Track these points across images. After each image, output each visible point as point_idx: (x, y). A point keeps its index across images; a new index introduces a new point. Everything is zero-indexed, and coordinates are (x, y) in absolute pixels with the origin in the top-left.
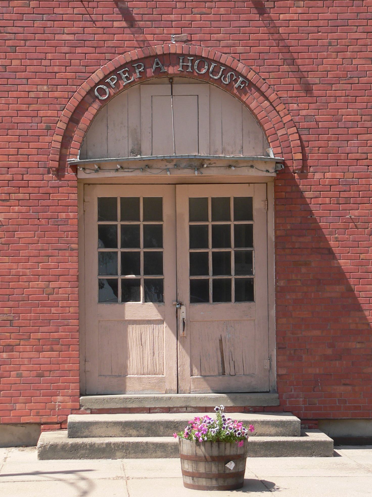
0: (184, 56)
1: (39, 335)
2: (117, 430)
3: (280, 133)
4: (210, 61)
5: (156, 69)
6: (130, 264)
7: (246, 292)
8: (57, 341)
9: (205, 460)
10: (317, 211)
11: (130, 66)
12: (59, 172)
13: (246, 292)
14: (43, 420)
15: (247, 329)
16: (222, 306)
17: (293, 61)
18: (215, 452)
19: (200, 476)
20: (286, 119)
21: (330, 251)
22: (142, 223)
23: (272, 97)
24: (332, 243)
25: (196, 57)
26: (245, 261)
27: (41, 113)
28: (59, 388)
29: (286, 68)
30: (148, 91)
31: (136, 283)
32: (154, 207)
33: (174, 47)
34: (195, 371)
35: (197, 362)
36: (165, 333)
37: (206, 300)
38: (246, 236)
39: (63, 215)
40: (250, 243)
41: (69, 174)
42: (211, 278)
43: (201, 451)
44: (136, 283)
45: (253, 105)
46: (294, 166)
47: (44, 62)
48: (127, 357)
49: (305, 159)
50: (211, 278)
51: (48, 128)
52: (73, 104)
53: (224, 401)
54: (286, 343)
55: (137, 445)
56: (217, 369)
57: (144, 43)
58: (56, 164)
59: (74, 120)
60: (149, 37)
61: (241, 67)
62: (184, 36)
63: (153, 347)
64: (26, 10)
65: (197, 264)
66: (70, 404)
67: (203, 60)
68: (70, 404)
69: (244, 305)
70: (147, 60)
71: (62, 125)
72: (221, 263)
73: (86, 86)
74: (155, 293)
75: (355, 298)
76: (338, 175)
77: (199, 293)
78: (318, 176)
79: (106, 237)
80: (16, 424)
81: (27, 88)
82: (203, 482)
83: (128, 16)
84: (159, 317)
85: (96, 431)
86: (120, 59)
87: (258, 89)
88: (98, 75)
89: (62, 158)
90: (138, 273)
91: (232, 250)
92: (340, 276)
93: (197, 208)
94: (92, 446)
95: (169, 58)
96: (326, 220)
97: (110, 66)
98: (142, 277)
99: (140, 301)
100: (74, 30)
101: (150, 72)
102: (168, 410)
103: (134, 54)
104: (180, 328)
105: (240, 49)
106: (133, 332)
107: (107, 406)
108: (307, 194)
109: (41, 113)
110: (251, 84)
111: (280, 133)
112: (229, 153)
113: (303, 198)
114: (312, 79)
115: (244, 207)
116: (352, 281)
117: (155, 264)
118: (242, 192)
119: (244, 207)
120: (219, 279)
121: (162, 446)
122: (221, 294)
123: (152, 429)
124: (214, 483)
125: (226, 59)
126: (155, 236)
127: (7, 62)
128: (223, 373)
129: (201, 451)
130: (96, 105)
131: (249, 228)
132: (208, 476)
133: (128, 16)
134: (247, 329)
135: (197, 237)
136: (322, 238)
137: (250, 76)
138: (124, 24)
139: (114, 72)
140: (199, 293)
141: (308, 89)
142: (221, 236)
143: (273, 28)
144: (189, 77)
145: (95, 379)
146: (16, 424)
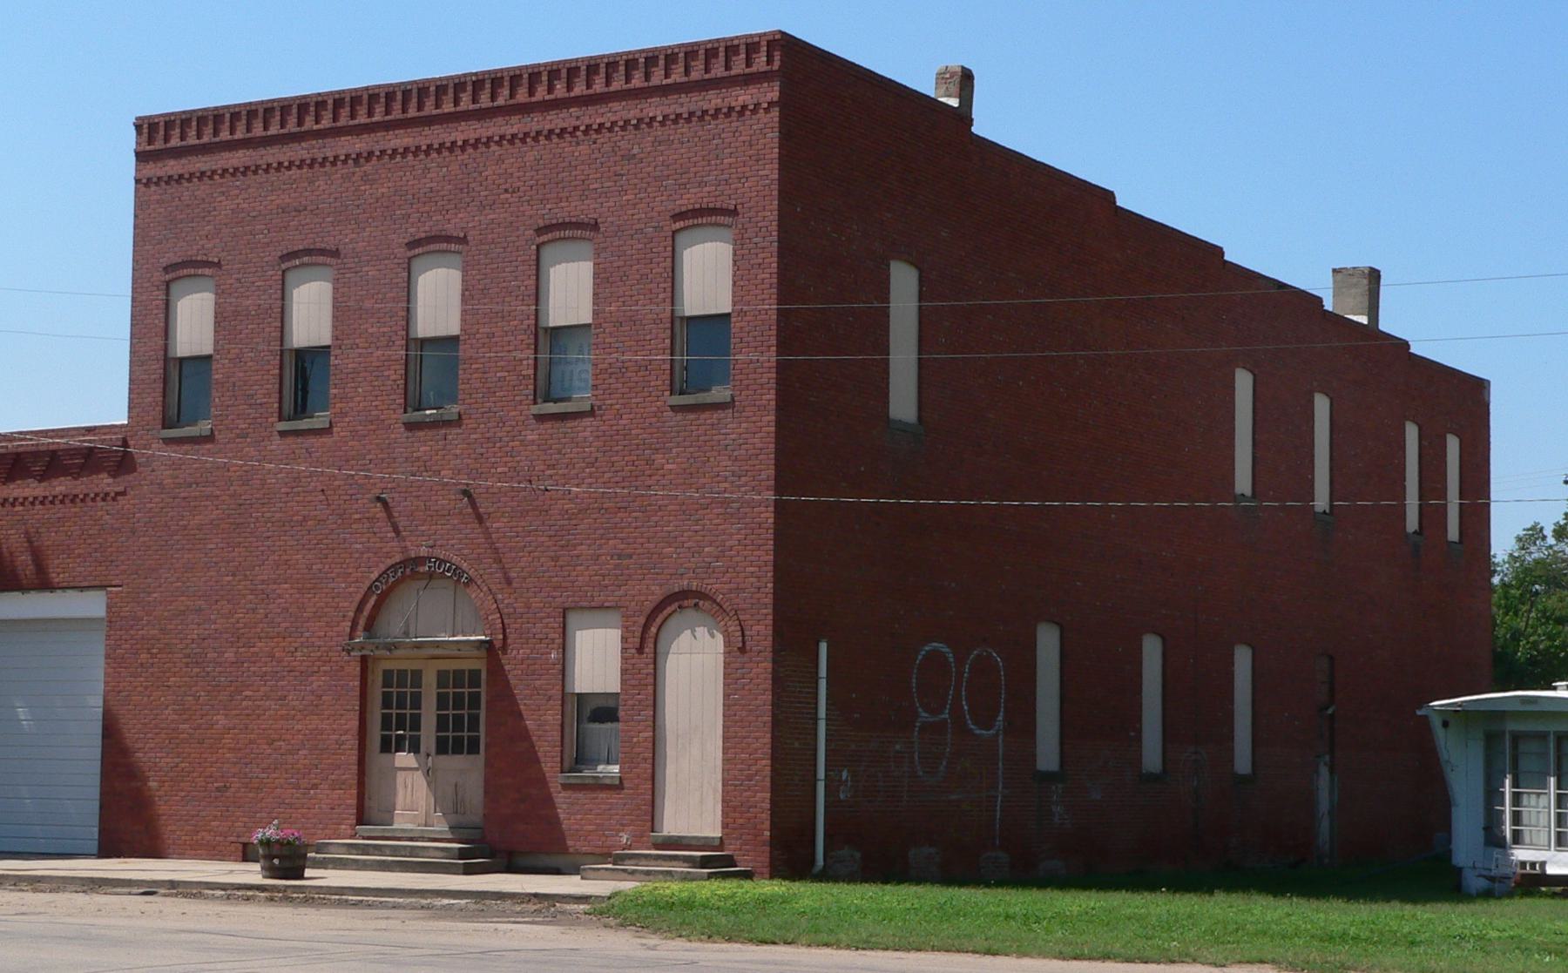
2: (344, 849)
13: (473, 748)
15: (468, 771)
21: (520, 715)
32: (417, 675)
33: (423, 551)
36: (419, 779)
46: (498, 644)
48: (395, 795)
52: (359, 597)
54: (491, 789)
61: (465, 566)
69: (472, 757)
71: (351, 614)
73: (367, 584)
74: (415, 748)
77: (442, 747)
83: (396, 531)
85: (332, 849)
86: (390, 562)
91: (465, 712)
93: (442, 677)
95: (420, 560)
96: (520, 691)
97: (383, 567)
99: (478, 752)
102: (411, 839)
103: (398, 558)
106: (400, 776)
118: (415, 666)
119: (474, 676)
122: (458, 749)
125: (456, 559)
135: (442, 702)
140: (442, 747)
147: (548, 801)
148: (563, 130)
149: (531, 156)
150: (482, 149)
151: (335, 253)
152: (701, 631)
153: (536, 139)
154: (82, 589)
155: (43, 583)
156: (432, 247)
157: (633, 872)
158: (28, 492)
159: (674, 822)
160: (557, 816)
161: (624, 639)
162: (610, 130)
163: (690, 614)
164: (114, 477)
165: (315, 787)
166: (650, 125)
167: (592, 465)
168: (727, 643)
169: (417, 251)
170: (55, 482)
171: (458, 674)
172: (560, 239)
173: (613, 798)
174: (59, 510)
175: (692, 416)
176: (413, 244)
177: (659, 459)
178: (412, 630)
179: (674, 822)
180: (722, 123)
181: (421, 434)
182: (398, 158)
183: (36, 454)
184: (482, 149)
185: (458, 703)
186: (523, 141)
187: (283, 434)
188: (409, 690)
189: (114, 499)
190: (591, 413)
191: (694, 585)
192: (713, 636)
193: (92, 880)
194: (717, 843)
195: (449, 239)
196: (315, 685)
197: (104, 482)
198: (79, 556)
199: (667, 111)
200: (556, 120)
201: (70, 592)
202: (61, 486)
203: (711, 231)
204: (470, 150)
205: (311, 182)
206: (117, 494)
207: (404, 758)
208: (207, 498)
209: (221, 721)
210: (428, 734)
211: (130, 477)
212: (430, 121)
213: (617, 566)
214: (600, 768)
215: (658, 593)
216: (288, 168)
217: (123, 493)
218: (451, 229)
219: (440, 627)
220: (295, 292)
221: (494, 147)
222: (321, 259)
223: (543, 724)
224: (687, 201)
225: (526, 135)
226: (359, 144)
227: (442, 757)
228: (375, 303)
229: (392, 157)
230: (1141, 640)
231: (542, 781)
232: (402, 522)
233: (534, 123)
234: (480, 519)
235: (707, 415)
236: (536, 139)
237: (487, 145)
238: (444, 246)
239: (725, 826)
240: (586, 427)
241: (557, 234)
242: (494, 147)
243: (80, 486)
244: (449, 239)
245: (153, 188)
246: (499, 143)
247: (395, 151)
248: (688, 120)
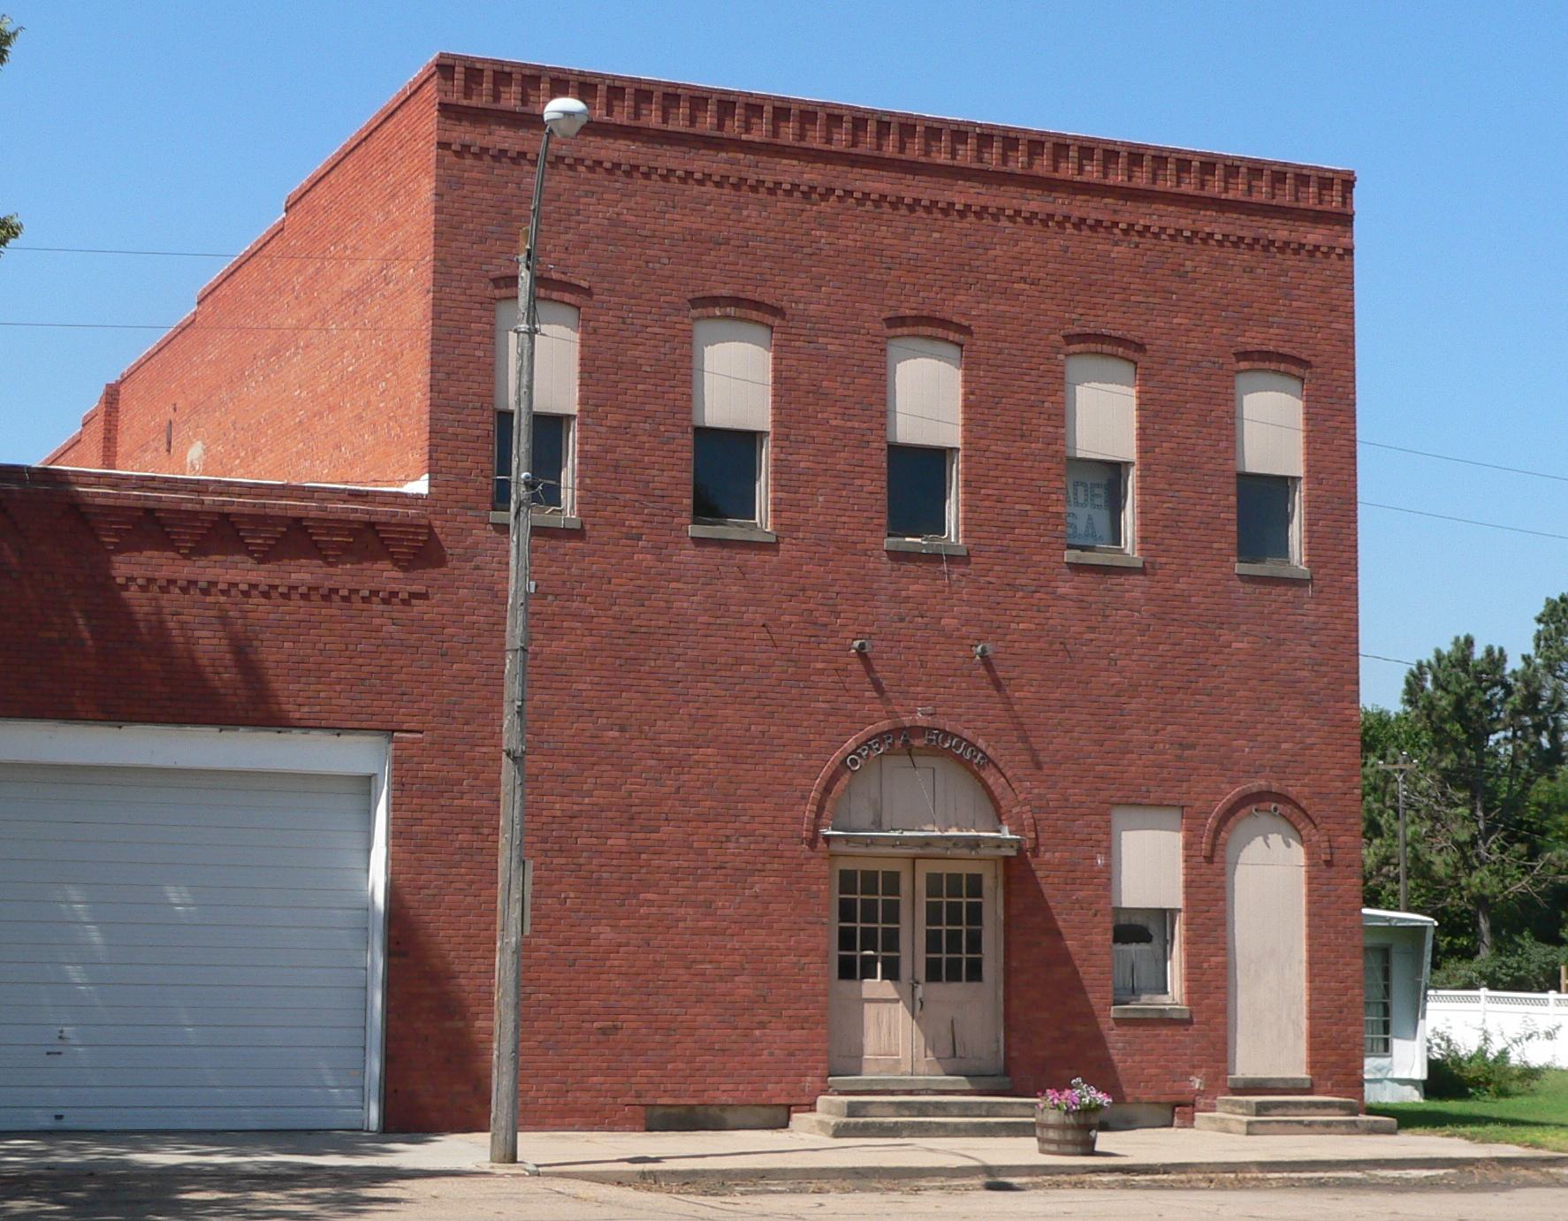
0: (930, 729)
1: (790, 1012)
2: (891, 1110)
3: (1015, 810)
4: (954, 735)
5: (904, 741)
6: (869, 940)
7: (975, 972)
8: (806, 1020)
9: (1072, 1127)
10: (1047, 890)
11: (880, 737)
12: (812, 843)
14: (794, 1101)
15: (975, 1008)
16: (955, 985)
17: (1025, 740)
18: (1082, 1121)
19: (1067, 1142)
20: (1021, 797)
22: (880, 898)
23: (1009, 774)
24: (1060, 923)
25: (942, 731)
26: (975, 943)
27: (796, 782)
28: (808, 1068)
29: (1020, 745)
30: (889, 762)
31: (874, 960)
32: (892, 880)
33: (920, 719)
34: (929, 1053)
35: (931, 1044)
37: (940, 980)
38: (976, 914)
39: (815, 888)
40: (979, 922)
41: (821, 845)
42: (944, 956)
43: (1071, 1120)
44: (874, 960)
45: (991, 781)
47: (800, 730)
49: (1037, 838)
50: (944, 956)
51: (803, 797)
52: (825, 772)
53: (962, 1082)
55: (956, 1125)
56: (949, 1052)
57: (891, 715)
58: (810, 835)
59: (827, 790)
60: (897, 708)
61: (981, 743)
62: (930, 709)
63: (891, 1029)
64: (784, 676)
65: (933, 941)
66: (819, 1085)
67: (947, 735)
68: (819, 1085)
69: (975, 985)
70: (897, 731)
72: (869, 915)
74: (892, 973)
75: (1080, 980)
76: (1067, 855)
77: (933, 974)
78: (1048, 855)
79: (846, 911)
80: (763, 1106)
81: (783, 755)
82: (1070, 1148)
83: (877, 686)
84: (896, 996)
85: (872, 1110)
87: (996, 766)
88: (851, 743)
89: (816, 831)
90: (875, 949)
91: (964, 928)
92: (1066, 958)
93: (934, 882)
94: (881, 1124)
98: (880, 954)
100: (828, 698)
101: (899, 743)
102: (910, 1093)
103: (884, 725)
104: (917, 1008)
105: (979, 724)
106: (870, 1011)
107: (942, 1087)
108: (1039, 874)
109: (796, 782)
110: (990, 760)
111: (1015, 810)
112: (540, 594)
113: (1035, 877)
114: (1042, 757)
115: (975, 884)
116: (1077, 963)
117: (892, 940)
118: (974, 868)
120: (952, 961)
121: (944, 1125)
122: (954, 976)
123: (922, 1109)
124: (1079, 1149)
125: (967, 734)
126: (892, 912)
127: (764, 728)
128: (954, 1055)
129: (1071, 1120)
130: (847, 776)
131: (979, 905)
132: (1073, 1143)
133: (877, 686)
134: (975, 1008)
135: (933, 914)
136: (1052, 919)
137: (990, 752)
138: (875, 694)
139: (865, 743)
140: (933, 974)
141: (1039, 766)
142: (954, 910)
143: (1008, 703)
144: (934, 751)
145: (839, 1061)
146: (763, 1106)
147: (1099, 1040)
148: (1099, 223)
149: (1057, 242)
150: (988, 220)
151: (777, 311)
152: (1276, 839)
153: (1061, 225)
154: (338, 730)
155: (261, 712)
156: (922, 330)
157: (1310, 1124)
158: (232, 575)
159: (1249, 1061)
160: (1109, 1059)
161: (1188, 846)
162: (1156, 236)
163: (1264, 819)
164: (405, 569)
165: (762, 1025)
166: (1204, 241)
167: (1142, 633)
168: (1310, 855)
169: (899, 331)
170: (290, 565)
171: (954, 879)
172: (1097, 353)
173: (1180, 1034)
174: (297, 609)
175: (1268, 589)
176: (892, 322)
177: (1226, 635)
178: (886, 819)
179: (1249, 1061)
180: (1290, 260)
181: (911, 566)
182: (869, 205)
183: (260, 520)
184: (988, 220)
185: (954, 917)
186: (1044, 223)
187: (699, 542)
188: (945, 900)
189: (405, 602)
190: (1142, 571)
191: (1275, 787)
192: (1288, 845)
193: (726, 1175)
194: (1307, 1085)
195: (944, 323)
196: (757, 889)
197: (386, 575)
198: (339, 681)
199: (1228, 229)
200: (1092, 209)
201: (315, 734)
202: (303, 573)
203: (1275, 379)
204: (971, 218)
205: (739, 208)
206: (413, 595)
207: (877, 986)
208: (575, 616)
209: (606, 933)
210: (913, 950)
211: (433, 573)
212: (913, 168)
213: (1179, 758)
214: (1145, 998)
215: (1233, 793)
216: (701, 182)
217: (424, 596)
218: (946, 312)
219: (926, 817)
220: (708, 351)
221: (1004, 223)
222: (754, 314)
223: (1086, 941)
224: (1253, 339)
225: (1051, 216)
226: (812, 175)
227: (934, 986)
228: (831, 388)
229: (860, 202)
230: (1109, 848)
231: (1089, 1016)
232: (886, 677)
233: (1060, 204)
234: (998, 684)
235: (1279, 590)
236: (1061, 225)
237: (995, 217)
238: (940, 332)
239: (1312, 1065)
240: (1135, 588)
241: (1092, 347)
242: (1004, 223)
243: (343, 575)
244: (944, 323)
245: (469, 161)
246: (1011, 218)
247: (866, 196)
248: (1251, 247)
